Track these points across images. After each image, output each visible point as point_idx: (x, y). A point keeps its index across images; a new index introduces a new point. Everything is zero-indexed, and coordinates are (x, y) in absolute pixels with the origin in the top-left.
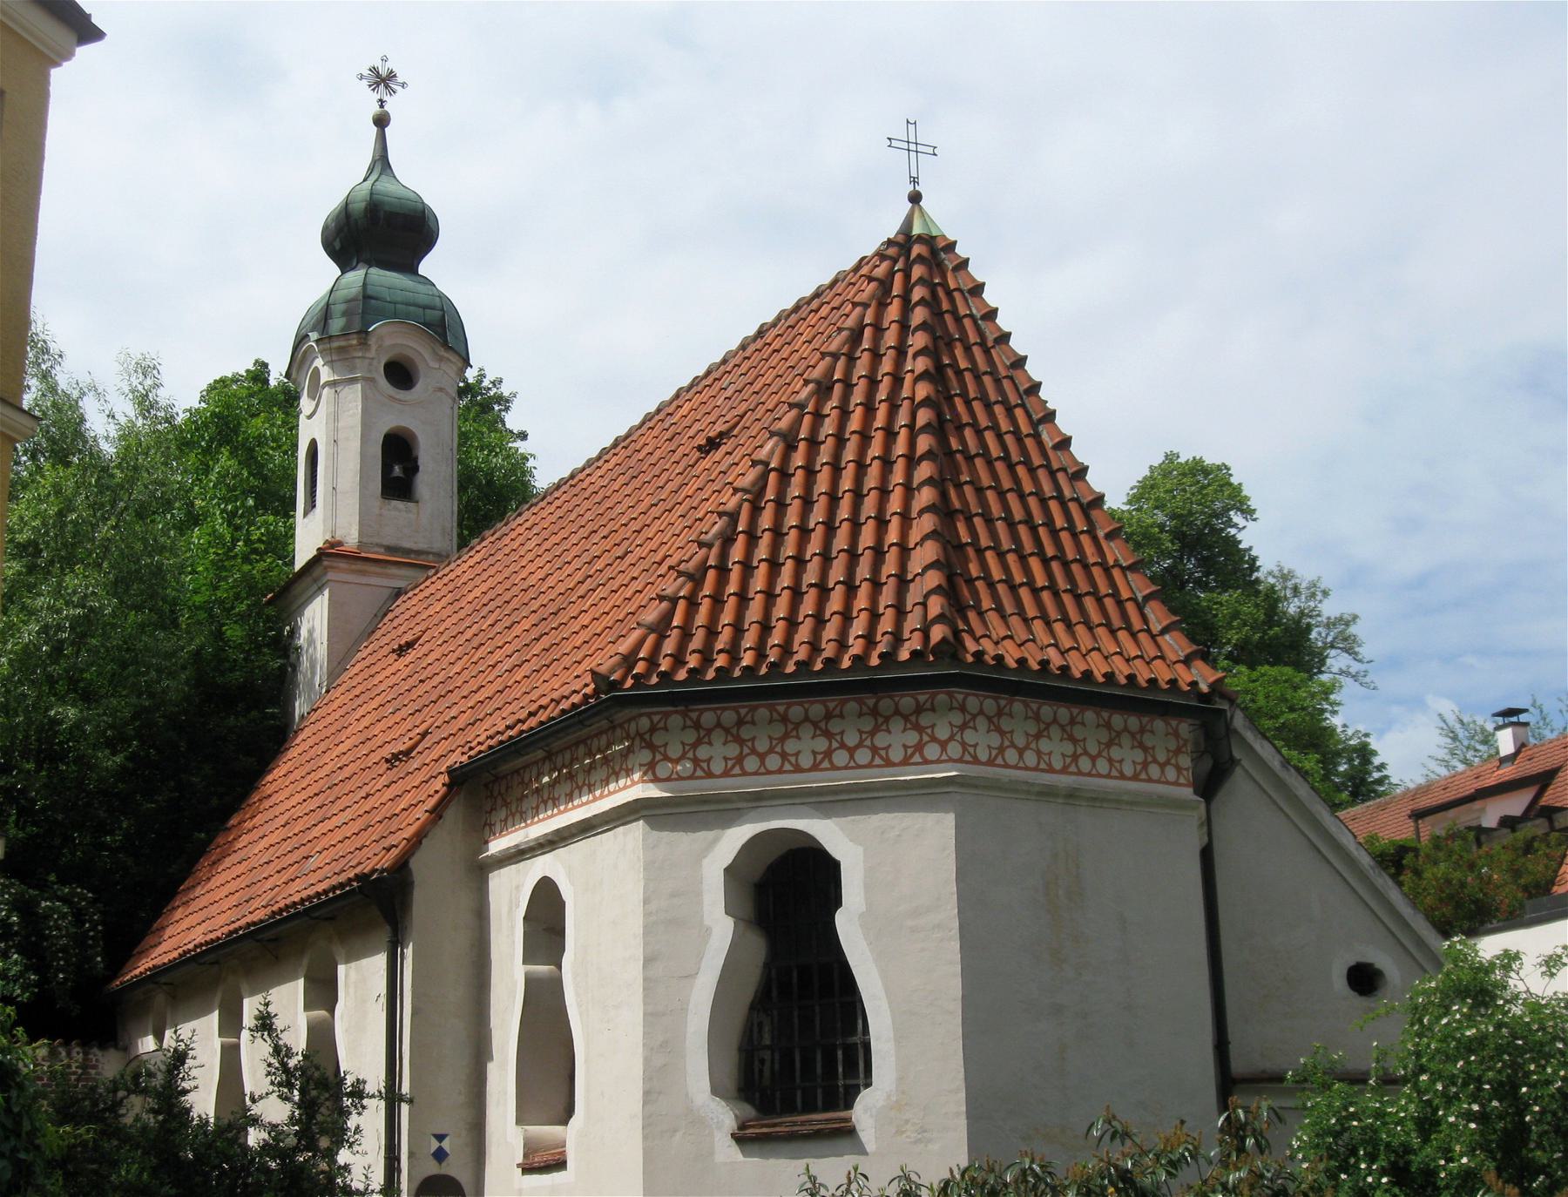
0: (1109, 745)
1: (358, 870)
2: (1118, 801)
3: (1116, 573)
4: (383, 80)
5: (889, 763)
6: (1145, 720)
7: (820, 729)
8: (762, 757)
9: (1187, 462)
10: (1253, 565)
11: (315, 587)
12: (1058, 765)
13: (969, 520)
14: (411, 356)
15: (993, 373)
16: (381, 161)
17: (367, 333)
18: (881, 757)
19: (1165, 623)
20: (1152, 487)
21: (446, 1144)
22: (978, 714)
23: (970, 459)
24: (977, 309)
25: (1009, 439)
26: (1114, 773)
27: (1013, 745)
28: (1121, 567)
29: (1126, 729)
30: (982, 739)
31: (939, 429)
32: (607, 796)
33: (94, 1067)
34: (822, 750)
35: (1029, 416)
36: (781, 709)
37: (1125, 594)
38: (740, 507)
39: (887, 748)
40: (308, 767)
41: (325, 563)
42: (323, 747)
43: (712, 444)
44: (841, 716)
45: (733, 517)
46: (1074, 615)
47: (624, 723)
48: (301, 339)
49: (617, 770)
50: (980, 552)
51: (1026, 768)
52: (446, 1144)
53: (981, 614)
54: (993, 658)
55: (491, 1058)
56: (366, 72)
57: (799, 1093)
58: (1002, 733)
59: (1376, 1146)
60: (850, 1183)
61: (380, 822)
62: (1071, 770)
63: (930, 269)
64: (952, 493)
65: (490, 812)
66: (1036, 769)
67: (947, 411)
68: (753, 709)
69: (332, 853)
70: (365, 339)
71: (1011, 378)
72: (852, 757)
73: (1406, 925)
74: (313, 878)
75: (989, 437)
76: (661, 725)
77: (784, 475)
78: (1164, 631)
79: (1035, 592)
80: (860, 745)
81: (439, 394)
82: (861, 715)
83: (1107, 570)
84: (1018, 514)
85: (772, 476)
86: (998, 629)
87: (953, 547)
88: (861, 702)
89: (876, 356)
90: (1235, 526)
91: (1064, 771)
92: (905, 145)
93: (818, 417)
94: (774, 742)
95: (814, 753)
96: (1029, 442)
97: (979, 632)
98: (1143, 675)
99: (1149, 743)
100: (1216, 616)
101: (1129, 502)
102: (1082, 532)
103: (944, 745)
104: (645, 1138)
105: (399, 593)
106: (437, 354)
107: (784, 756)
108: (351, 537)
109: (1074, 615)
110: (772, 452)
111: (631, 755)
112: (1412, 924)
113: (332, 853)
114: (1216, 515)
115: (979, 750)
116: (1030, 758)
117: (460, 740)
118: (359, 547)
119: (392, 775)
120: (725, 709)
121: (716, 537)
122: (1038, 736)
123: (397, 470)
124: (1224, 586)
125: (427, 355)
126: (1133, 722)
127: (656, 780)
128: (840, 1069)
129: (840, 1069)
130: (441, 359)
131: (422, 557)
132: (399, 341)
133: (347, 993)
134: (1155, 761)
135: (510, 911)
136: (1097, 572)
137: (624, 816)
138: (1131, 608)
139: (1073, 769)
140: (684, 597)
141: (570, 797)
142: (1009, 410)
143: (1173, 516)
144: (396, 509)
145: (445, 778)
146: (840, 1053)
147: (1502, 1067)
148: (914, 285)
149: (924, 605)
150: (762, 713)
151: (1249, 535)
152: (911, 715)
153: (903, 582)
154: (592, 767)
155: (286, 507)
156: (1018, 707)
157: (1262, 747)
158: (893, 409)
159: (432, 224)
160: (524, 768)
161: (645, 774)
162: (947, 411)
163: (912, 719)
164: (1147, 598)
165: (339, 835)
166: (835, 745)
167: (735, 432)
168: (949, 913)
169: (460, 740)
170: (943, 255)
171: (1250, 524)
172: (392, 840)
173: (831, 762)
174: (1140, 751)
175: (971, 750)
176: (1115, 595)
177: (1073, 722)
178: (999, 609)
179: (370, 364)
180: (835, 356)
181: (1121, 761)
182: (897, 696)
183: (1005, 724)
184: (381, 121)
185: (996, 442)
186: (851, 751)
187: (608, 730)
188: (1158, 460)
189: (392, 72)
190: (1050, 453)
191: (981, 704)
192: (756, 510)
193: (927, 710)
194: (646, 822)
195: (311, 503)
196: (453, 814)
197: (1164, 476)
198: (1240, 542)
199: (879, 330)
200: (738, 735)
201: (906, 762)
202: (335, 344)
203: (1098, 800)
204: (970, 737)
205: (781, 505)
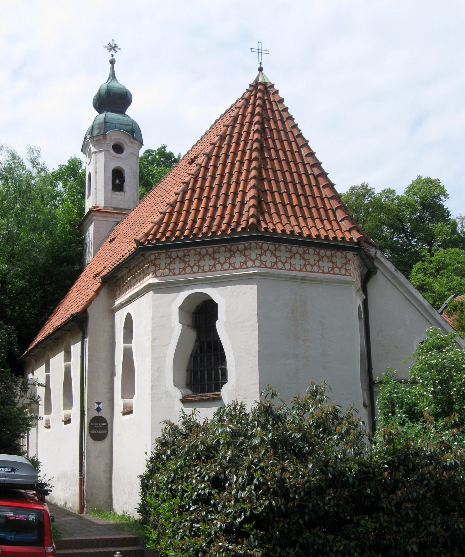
2: (322, 281)
3: (326, 200)
4: (113, 48)
5: (235, 268)
6: (333, 252)
8: (192, 267)
9: (425, 179)
10: (449, 215)
11: (90, 223)
12: (298, 268)
13: (269, 182)
14: (121, 141)
15: (285, 130)
16: (113, 76)
17: (105, 134)
19: (342, 217)
20: (413, 188)
21: (101, 406)
22: (267, 250)
23: (272, 160)
24: (281, 108)
25: (288, 153)
27: (281, 261)
30: (269, 259)
31: (261, 150)
35: (297, 144)
36: (198, 250)
37: (328, 207)
38: (190, 180)
41: (92, 214)
44: (219, 252)
45: (187, 184)
46: (307, 215)
48: (86, 138)
50: (272, 193)
51: (286, 269)
53: (270, 215)
54: (272, 230)
55: (115, 375)
56: (107, 45)
57: (206, 386)
58: (276, 257)
59: (402, 404)
60: (193, 414)
63: (264, 94)
64: (263, 172)
66: (290, 270)
67: (264, 143)
68: (189, 251)
71: (292, 132)
72: (222, 266)
75: (281, 153)
76: (158, 257)
77: (206, 169)
78: (342, 220)
79: (293, 207)
80: (225, 262)
82: (225, 251)
83: (322, 199)
84: (289, 179)
85: (202, 169)
86: (276, 219)
87: (262, 191)
88: (225, 247)
89: (242, 125)
90: (442, 200)
93: (220, 147)
96: (296, 154)
97: (268, 220)
98: (331, 235)
99: (334, 260)
100: (434, 231)
101: (405, 193)
102: (314, 186)
103: (254, 261)
104: (152, 401)
105: (118, 223)
107: (199, 267)
108: (101, 205)
109: (307, 215)
110: (203, 161)
112: (445, 327)
114: (435, 197)
116: (287, 266)
118: (104, 208)
120: (179, 251)
121: (181, 191)
122: (291, 258)
123: (117, 182)
124: (439, 221)
125: (127, 142)
126: (328, 253)
127: (156, 277)
128: (220, 377)
129: (220, 377)
130: (132, 143)
131: (127, 211)
132: (116, 137)
136: (318, 200)
137: (147, 290)
138: (330, 212)
139: (304, 270)
140: (168, 212)
141: (135, 285)
142: (290, 144)
143: (421, 198)
144: (117, 194)
146: (220, 372)
147: (446, 375)
148: (257, 100)
149: (248, 211)
151: (447, 204)
153: (243, 204)
154: (140, 273)
155: (83, 197)
156: (283, 248)
157: (387, 263)
158: (246, 143)
159: (129, 97)
160: (124, 276)
161: (153, 274)
162: (264, 143)
163: (243, 253)
164: (336, 209)
166: (217, 262)
168: (254, 321)
170: (269, 89)
171: (447, 199)
173: (215, 268)
175: (264, 263)
176: (324, 208)
177: (304, 253)
178: (278, 213)
180: (228, 126)
181: (323, 267)
183: (278, 254)
184: (112, 62)
185: (283, 154)
186: (222, 264)
188: (415, 178)
190: (304, 158)
192: (196, 181)
194: (153, 291)
195: (89, 194)
196: (103, 293)
197: (417, 184)
198: (444, 206)
199: (244, 116)
201: (241, 268)
202: (95, 139)
203: (313, 281)
204: (263, 258)
205: (204, 179)
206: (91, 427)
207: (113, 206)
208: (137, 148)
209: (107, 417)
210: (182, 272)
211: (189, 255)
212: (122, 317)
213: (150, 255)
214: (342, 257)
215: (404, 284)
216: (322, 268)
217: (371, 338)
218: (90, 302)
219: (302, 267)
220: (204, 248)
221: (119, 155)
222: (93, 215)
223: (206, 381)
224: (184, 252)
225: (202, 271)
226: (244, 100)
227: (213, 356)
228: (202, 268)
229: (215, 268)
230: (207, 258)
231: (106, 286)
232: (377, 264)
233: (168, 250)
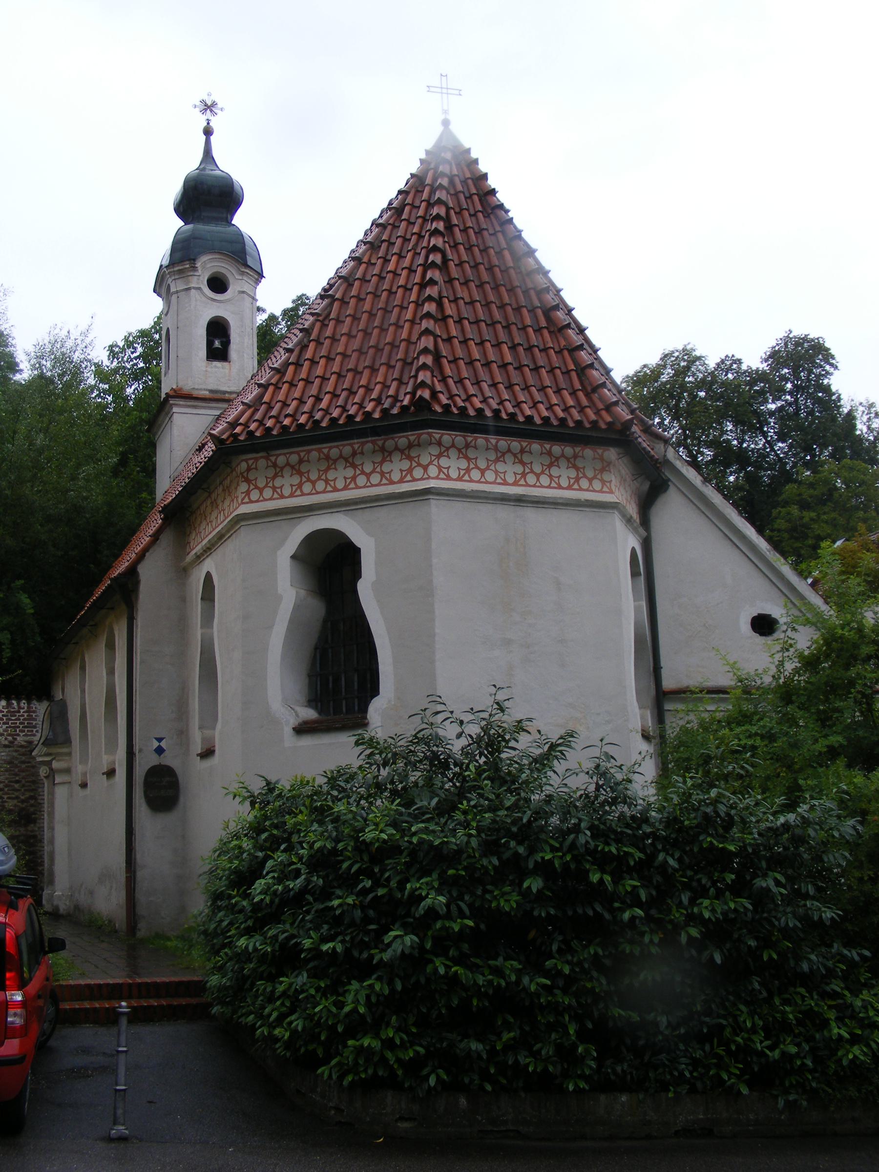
4: (208, 107)
6: (577, 449)
18: (386, 479)
21: (163, 744)
22: (450, 447)
26: (553, 484)
29: (563, 455)
33: (34, 712)
36: (325, 451)
39: (389, 473)
56: (198, 103)
62: (520, 483)
72: (368, 480)
73: (793, 589)
76: (254, 466)
80: (373, 471)
82: (374, 452)
91: (516, 483)
99: (580, 465)
107: (327, 481)
123: (217, 344)
130: (243, 273)
144: (216, 367)
166: (358, 472)
173: (355, 484)
177: (522, 451)
184: (208, 132)
196: (166, 539)
207: (210, 388)
210: (296, 491)
211: (308, 461)
212: (199, 580)
213: (239, 464)
214: (594, 459)
215: (720, 508)
216: (556, 480)
217: (658, 610)
219: (518, 477)
220: (335, 447)
221: (219, 297)
222: (172, 405)
223: (344, 694)
224: (299, 456)
228: (332, 483)
229: (355, 484)
230: (287, 472)
232: (668, 474)
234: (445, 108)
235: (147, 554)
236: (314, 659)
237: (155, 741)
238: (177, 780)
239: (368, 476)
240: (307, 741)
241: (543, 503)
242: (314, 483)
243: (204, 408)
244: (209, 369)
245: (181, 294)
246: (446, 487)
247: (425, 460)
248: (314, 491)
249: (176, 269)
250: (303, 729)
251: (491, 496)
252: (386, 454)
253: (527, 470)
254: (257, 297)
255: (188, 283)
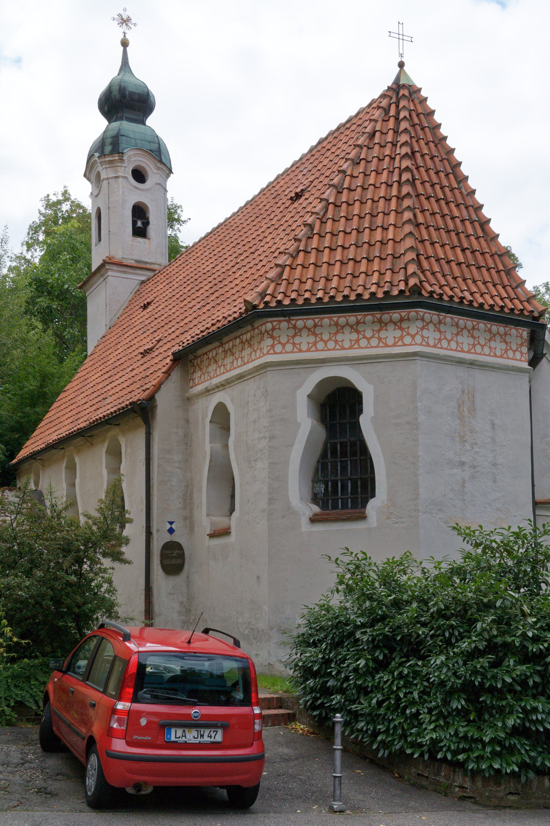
0: (490, 340)
1: (131, 401)
4: (125, 21)
6: (507, 329)
7: (354, 329)
12: (466, 349)
21: (174, 526)
22: (430, 323)
27: (445, 338)
28: (498, 254)
29: (498, 333)
32: (251, 362)
34: (355, 339)
36: (335, 319)
39: (386, 338)
40: (103, 361)
41: (107, 267)
42: (109, 352)
43: (298, 196)
47: (259, 326)
48: (90, 156)
49: (255, 349)
52: (174, 526)
56: (116, 17)
57: (340, 501)
61: (140, 380)
65: (193, 374)
69: (117, 396)
70: (122, 157)
72: (369, 342)
74: (108, 407)
76: (277, 327)
81: (158, 186)
87: (419, 241)
92: (397, 36)
94: (332, 335)
95: (351, 340)
99: (508, 341)
106: (156, 165)
107: (336, 342)
111: (263, 342)
113: (117, 396)
115: (429, 339)
116: (453, 345)
117: (178, 341)
119: (145, 359)
121: (303, 236)
123: (139, 224)
129: (359, 490)
130: (158, 168)
133: (126, 458)
134: (511, 349)
135: (203, 419)
139: (473, 351)
144: (139, 242)
145: (171, 357)
149: (405, 268)
150: (326, 321)
152: (398, 322)
165: (120, 388)
166: (361, 336)
167: (309, 189)
169: (178, 341)
172: (147, 386)
173: (359, 345)
174: (504, 344)
175: (426, 339)
179: (125, 170)
182: (391, 313)
184: (125, 44)
187: (251, 330)
189: (129, 17)
191: (431, 317)
193: (405, 320)
196: (176, 375)
200: (314, 332)
206: (163, 556)
208: (164, 177)
209: (182, 541)
218: (158, 387)
219: (471, 347)
220: (342, 316)
221: (140, 186)
222: (107, 269)
223: (340, 495)
225: (297, 351)
226: (380, 110)
227: (349, 462)
229: (359, 345)
230: (305, 332)
231: (179, 365)
233: (292, 318)
234: (401, 52)
235: (162, 386)
236: (317, 470)
237: (168, 524)
238: (184, 553)
239: (369, 339)
240: (320, 528)
241: (486, 366)
242: (326, 342)
243: (131, 273)
244: (134, 244)
245: (111, 181)
246: (428, 351)
247: (413, 331)
248: (326, 349)
249: (107, 159)
250: (314, 520)
251: (455, 360)
252: (383, 325)
253: (476, 342)
254: (167, 189)
255: (116, 172)
